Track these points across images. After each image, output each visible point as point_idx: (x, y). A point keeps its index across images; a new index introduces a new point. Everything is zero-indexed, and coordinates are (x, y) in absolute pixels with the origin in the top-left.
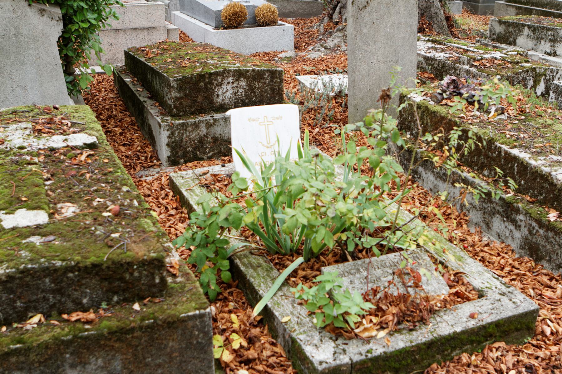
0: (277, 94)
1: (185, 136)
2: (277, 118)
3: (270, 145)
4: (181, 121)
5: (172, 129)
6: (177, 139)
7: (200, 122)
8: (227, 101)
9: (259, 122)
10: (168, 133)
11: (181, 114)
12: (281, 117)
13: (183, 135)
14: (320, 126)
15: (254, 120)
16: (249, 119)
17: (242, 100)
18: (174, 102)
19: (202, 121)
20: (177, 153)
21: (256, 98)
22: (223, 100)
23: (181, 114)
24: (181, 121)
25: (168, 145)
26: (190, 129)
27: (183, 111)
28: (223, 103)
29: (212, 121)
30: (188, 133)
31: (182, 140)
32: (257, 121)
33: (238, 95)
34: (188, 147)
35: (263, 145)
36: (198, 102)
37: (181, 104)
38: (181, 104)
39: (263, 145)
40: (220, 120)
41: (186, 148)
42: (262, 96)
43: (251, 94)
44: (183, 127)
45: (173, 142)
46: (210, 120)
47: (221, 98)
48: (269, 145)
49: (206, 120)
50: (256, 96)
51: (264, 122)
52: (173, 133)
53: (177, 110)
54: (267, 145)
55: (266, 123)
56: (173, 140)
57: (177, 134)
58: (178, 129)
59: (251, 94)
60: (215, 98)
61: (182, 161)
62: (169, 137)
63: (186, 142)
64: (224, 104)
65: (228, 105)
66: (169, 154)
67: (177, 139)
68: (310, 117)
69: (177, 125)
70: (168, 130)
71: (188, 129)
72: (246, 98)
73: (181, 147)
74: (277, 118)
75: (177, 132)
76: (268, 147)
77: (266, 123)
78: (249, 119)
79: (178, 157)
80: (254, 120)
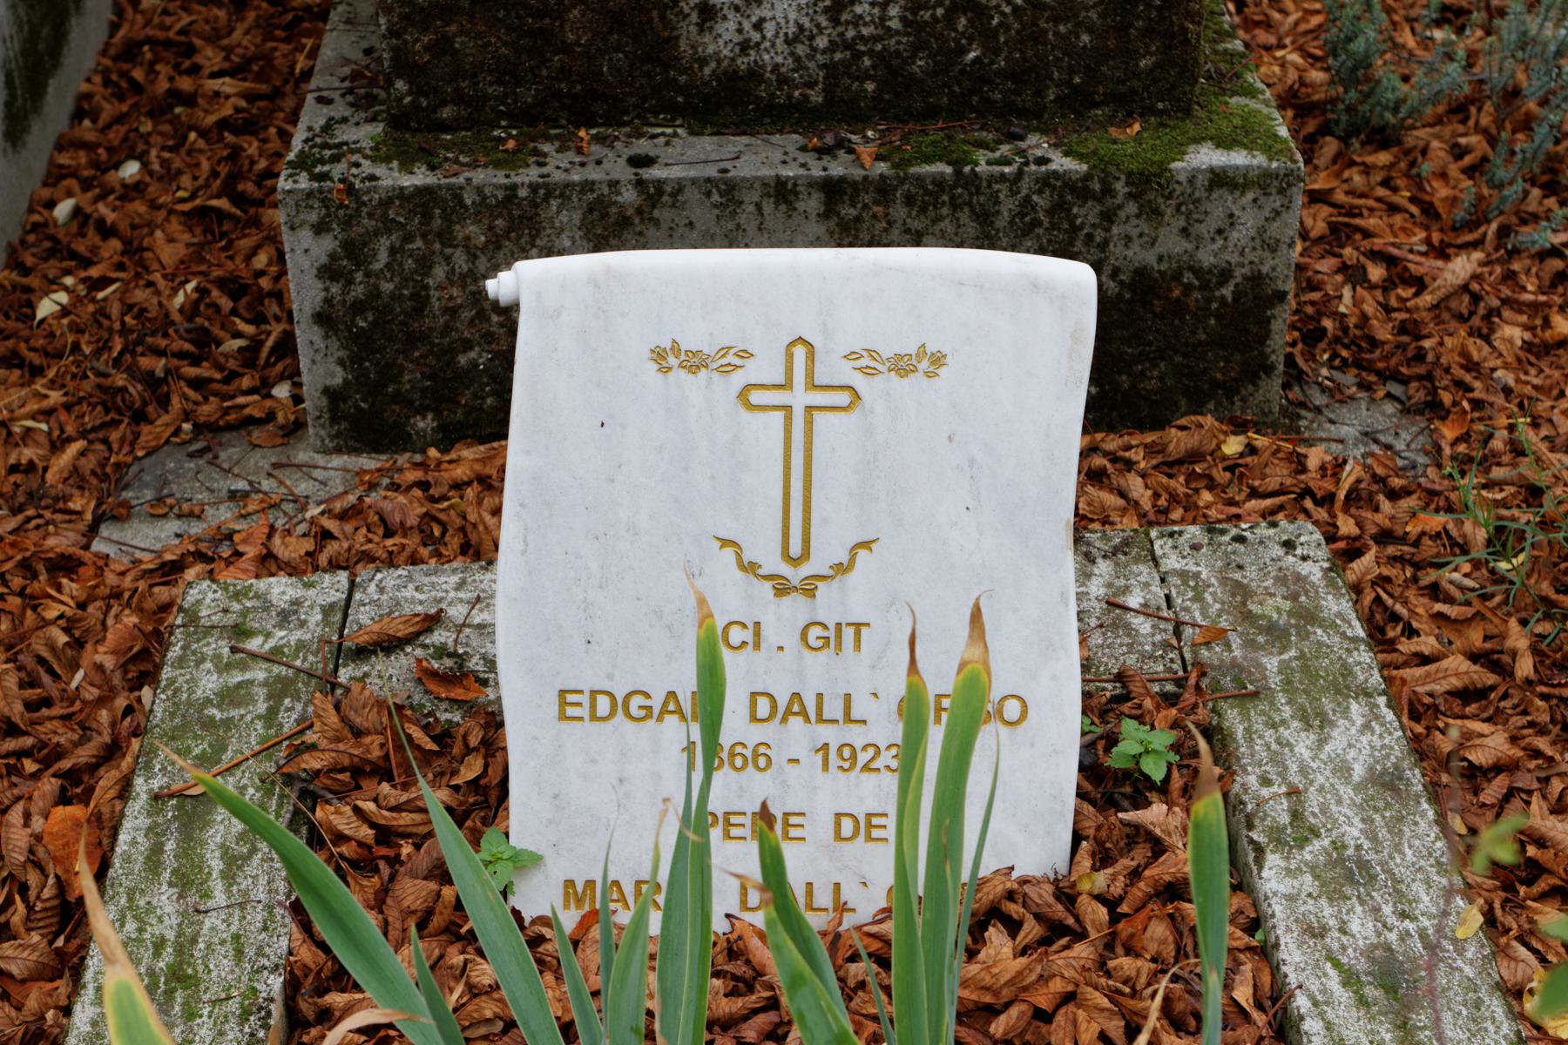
0: (1147, 33)
1: (439, 272)
2: (902, 366)
3: (806, 569)
4: (421, 177)
5: (347, 223)
6: (387, 287)
7: (544, 192)
8: (774, 56)
9: (738, 379)
10: (326, 245)
11: (446, 113)
12: (938, 360)
13: (425, 265)
14: (1504, 232)
15: (695, 363)
16: (659, 355)
17: (881, 58)
18: (393, 32)
19: (564, 192)
20: (390, 373)
21: (992, 50)
22: (745, 46)
23: (446, 113)
24: (421, 177)
25: (322, 318)
26: (474, 231)
27: (459, 99)
28: (742, 63)
29: (629, 196)
30: (460, 260)
31: (420, 302)
32: (728, 370)
33: (857, 21)
34: (468, 346)
35: (750, 568)
36: (566, 49)
37: (442, 46)
38: (442, 46)
39: (750, 568)
40: (692, 195)
41: (451, 351)
42: (1038, 37)
43: (950, 19)
44: (427, 216)
45: (358, 308)
46: (614, 184)
47: (728, 29)
48: (795, 575)
49: (588, 186)
50: (988, 37)
51: (787, 385)
52: (355, 251)
53: (417, 91)
54: (785, 569)
55: (800, 398)
56: (358, 291)
57: (384, 257)
58: (388, 226)
59: (950, 19)
60: (688, 30)
61: (425, 424)
62: (328, 272)
63: (453, 312)
64: (755, 74)
65: (783, 80)
66: (338, 377)
67: (387, 287)
68: (1458, 152)
69: (386, 203)
70: (319, 229)
71: (460, 232)
72: (916, 49)
73: (412, 340)
74: (902, 366)
75: (383, 245)
76: (782, 589)
77: (800, 398)
78: (659, 355)
79: (397, 397)
80: (695, 363)
